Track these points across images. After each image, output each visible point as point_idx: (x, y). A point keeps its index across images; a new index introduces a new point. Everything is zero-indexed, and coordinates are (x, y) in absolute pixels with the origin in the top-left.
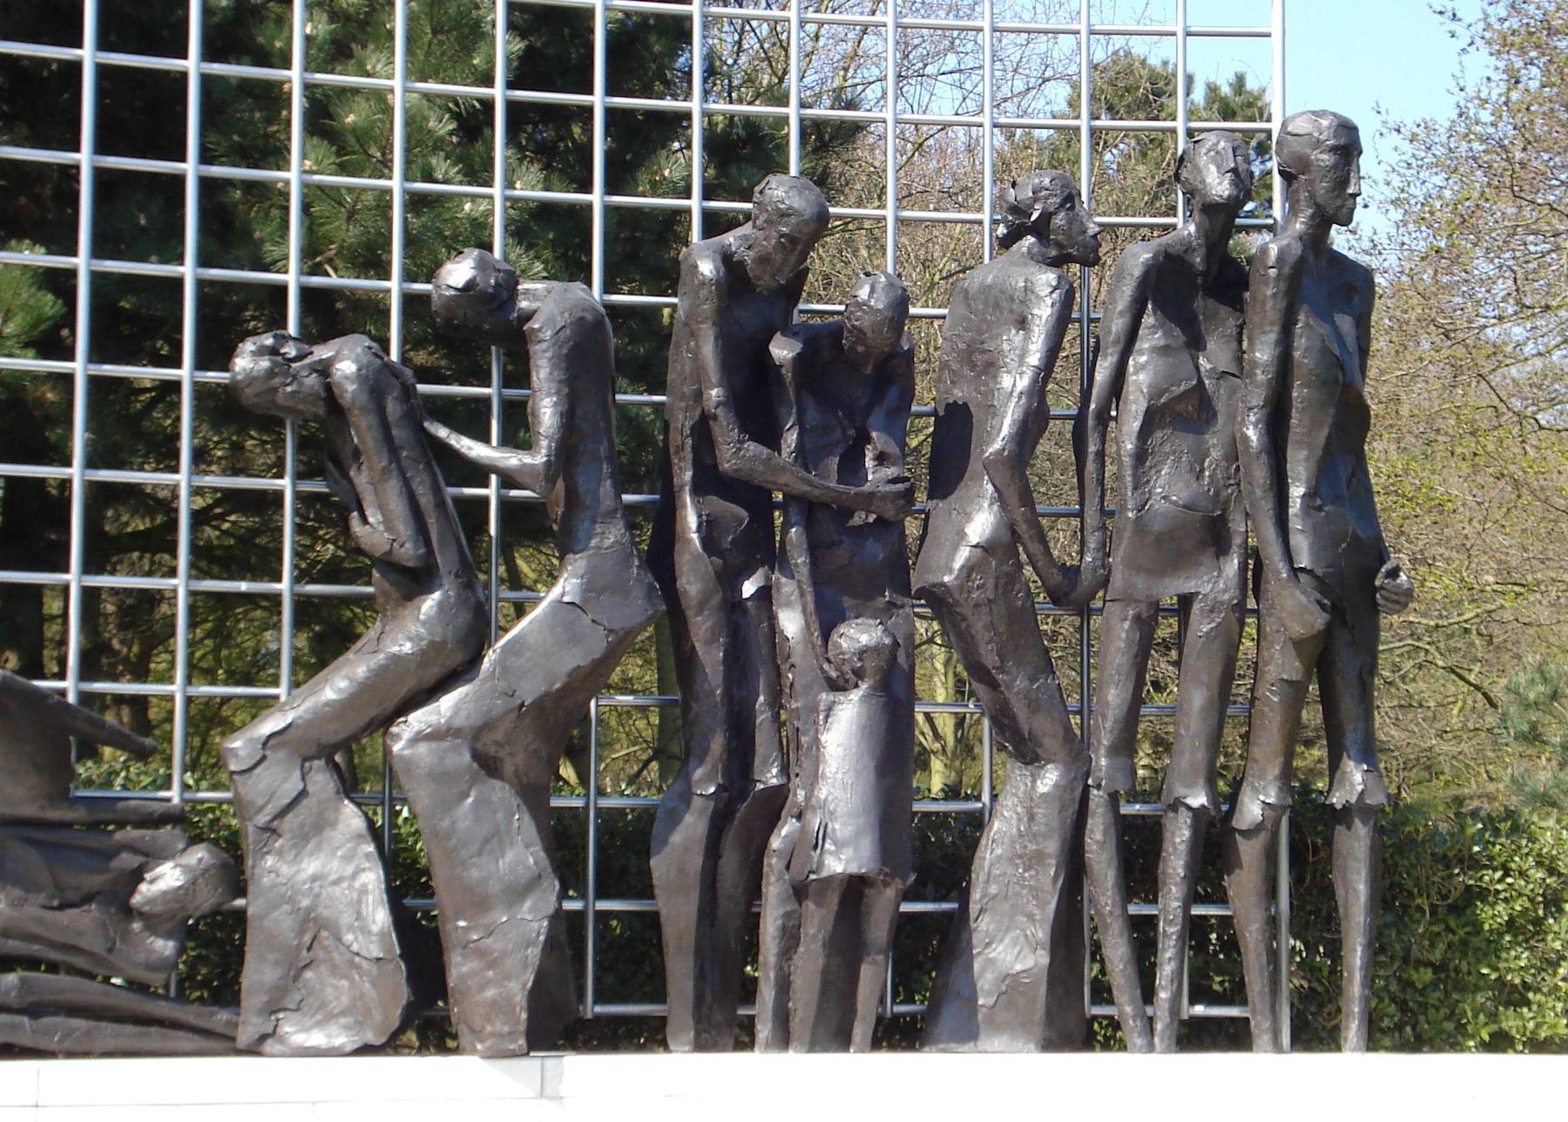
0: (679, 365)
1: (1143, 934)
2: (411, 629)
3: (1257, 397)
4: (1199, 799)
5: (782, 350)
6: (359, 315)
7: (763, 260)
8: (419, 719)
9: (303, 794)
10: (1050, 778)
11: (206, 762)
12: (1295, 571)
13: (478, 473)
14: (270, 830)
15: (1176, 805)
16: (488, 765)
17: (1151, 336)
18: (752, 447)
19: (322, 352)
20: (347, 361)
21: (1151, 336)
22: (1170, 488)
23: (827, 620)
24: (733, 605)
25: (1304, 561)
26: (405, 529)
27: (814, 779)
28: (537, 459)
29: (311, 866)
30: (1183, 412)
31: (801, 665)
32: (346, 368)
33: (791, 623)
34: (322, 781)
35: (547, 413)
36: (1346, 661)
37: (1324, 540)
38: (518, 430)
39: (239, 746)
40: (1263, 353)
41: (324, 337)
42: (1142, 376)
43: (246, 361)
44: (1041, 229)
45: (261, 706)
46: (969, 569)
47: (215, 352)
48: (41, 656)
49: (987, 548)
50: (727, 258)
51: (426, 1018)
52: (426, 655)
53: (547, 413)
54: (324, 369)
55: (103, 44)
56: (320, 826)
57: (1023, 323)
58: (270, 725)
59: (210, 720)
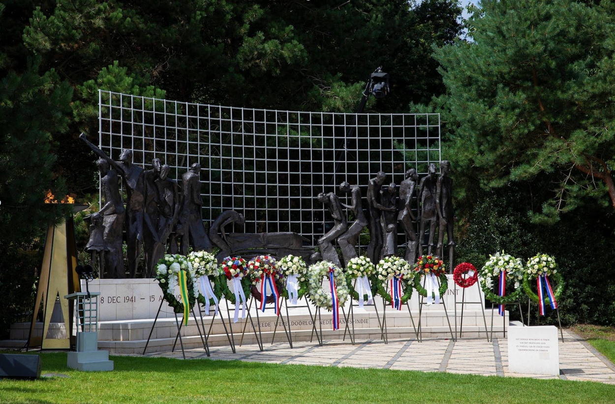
0: (368, 194)
2: (339, 227)
3: (438, 196)
4: (432, 244)
5: (381, 192)
6: (331, 189)
7: (379, 182)
9: (328, 246)
10: (414, 243)
11: (316, 243)
12: (443, 217)
13: (345, 208)
14: (325, 250)
15: (429, 245)
16: (349, 242)
17: (425, 189)
18: (378, 204)
19: (328, 195)
20: (332, 195)
21: (425, 189)
22: (428, 207)
23: (387, 225)
24: (376, 223)
26: (339, 216)
27: (386, 243)
28: (354, 207)
29: (329, 254)
30: (429, 199)
31: (384, 231)
32: (332, 197)
33: (383, 225)
34: (330, 245)
35: (354, 202)
36: (450, 227)
37: (447, 213)
38: (350, 203)
39: (320, 240)
40: (438, 191)
41: (328, 193)
42: (424, 193)
43: (319, 196)
44: (412, 176)
45: (322, 236)
46: (404, 218)
47: (315, 194)
48: (183, 244)
49: (406, 215)
50: (374, 182)
52: (341, 230)
53: (354, 202)
54: (329, 197)
55: (112, 132)
56: (330, 249)
57: (410, 188)
58: (324, 238)
59: (317, 237)
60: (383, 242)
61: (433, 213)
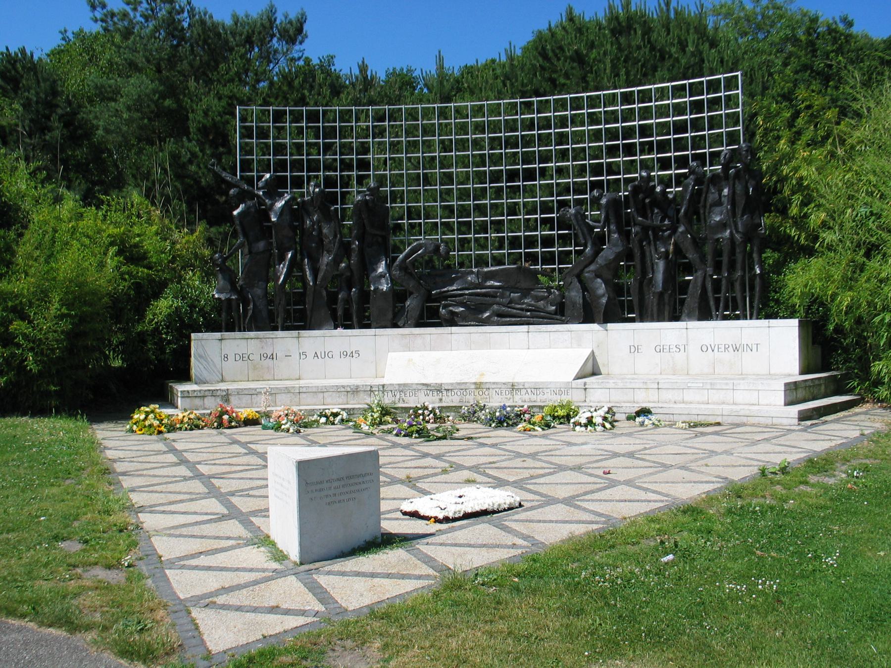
1: (717, 301)
8: (587, 270)
25: (740, 230)
51: (588, 318)
60: (653, 273)
61: (723, 226)
